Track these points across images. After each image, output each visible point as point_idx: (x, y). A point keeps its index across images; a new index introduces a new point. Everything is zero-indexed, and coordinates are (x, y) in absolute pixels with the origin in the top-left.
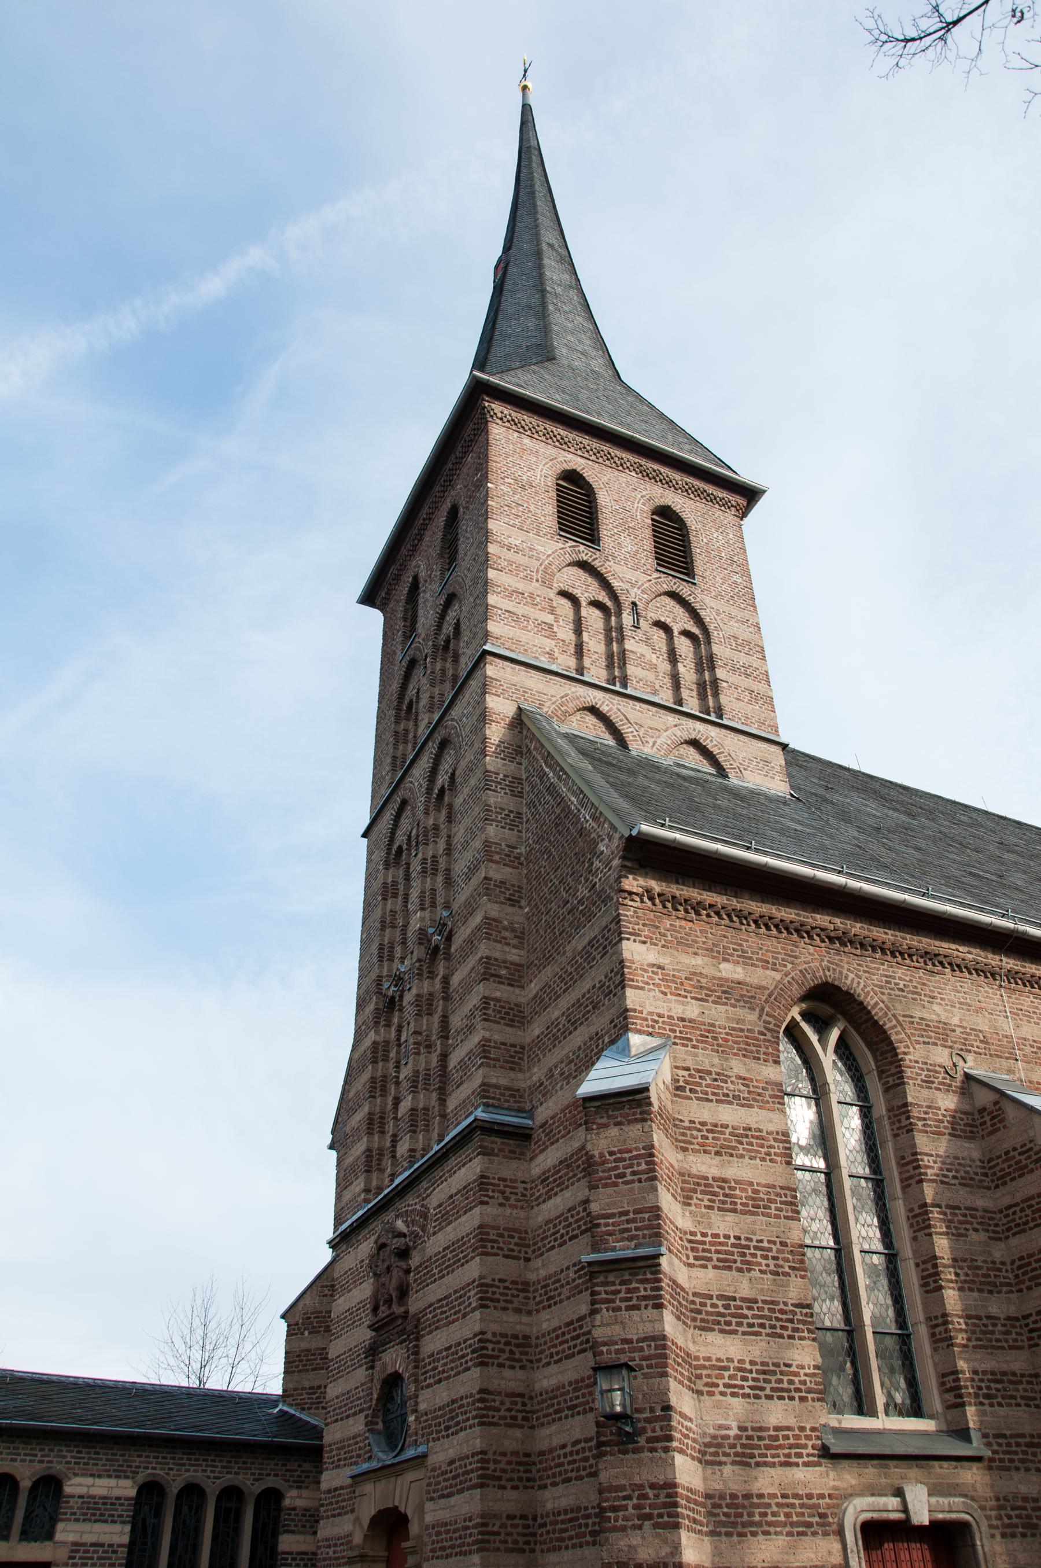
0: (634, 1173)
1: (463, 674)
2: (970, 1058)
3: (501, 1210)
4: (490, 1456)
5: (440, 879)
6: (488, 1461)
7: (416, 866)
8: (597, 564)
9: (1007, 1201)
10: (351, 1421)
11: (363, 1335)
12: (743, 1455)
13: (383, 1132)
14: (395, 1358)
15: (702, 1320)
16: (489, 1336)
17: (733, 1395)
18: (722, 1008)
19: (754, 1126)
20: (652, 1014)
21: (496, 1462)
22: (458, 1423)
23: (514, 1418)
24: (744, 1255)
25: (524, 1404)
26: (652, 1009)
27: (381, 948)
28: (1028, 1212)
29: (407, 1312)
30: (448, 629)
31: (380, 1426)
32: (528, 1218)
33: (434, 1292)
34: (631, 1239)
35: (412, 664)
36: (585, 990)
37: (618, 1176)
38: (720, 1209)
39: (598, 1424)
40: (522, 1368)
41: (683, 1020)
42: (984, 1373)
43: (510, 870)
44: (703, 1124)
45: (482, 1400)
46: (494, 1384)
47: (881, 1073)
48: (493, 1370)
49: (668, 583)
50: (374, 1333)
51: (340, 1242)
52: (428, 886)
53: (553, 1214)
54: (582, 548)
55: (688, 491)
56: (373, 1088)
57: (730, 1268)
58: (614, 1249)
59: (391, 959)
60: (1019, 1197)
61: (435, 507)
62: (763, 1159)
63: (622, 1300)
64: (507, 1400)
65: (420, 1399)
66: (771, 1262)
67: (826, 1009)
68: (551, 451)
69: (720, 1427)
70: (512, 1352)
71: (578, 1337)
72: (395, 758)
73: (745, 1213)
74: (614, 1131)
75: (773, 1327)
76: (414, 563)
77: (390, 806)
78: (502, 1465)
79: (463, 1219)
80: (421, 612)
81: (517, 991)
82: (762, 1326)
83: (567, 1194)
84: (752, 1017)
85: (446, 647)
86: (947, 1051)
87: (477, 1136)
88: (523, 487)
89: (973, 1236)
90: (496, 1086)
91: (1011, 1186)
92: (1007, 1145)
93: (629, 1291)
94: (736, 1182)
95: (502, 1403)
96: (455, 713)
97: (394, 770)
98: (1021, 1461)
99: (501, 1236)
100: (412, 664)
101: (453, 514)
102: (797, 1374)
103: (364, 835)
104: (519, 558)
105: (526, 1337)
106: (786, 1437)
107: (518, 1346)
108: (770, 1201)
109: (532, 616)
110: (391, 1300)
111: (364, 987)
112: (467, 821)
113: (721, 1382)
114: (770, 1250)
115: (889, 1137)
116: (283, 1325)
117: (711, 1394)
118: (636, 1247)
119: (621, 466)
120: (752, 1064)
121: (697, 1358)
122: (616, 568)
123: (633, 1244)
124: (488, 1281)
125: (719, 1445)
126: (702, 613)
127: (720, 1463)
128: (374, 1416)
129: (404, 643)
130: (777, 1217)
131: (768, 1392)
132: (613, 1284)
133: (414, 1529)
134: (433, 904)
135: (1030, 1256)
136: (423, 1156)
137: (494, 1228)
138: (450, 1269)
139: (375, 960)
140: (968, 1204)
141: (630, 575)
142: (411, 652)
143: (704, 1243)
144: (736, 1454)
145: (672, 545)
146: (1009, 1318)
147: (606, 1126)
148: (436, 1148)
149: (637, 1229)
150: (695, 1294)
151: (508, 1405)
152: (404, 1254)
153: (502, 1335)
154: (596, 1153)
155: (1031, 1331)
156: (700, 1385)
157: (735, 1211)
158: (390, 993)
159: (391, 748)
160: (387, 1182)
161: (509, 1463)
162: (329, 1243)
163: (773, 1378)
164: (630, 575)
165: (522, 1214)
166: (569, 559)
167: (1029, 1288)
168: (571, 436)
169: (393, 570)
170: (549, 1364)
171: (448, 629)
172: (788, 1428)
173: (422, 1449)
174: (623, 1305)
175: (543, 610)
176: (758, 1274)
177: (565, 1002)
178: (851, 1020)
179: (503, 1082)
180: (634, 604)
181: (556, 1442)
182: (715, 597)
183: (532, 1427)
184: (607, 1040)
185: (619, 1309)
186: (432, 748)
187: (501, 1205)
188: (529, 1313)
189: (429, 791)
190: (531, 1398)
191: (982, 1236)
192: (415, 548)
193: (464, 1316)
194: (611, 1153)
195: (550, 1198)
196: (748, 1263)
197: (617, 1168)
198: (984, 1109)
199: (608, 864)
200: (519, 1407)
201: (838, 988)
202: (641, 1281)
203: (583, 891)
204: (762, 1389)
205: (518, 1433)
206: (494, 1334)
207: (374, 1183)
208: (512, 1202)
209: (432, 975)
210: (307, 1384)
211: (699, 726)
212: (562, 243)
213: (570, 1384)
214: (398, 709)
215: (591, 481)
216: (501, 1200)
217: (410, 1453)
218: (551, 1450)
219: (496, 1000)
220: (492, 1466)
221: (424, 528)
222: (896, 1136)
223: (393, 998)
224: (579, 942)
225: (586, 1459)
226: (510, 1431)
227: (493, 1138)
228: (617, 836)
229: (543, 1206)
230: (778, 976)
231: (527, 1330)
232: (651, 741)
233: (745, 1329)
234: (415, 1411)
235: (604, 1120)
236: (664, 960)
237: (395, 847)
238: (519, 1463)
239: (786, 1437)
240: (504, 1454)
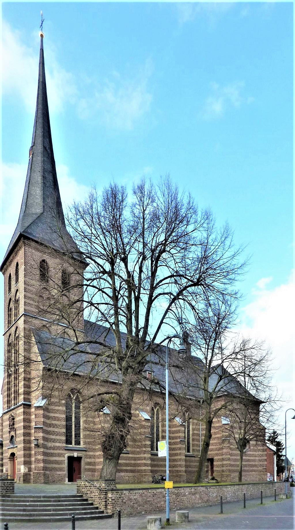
14: (13, 433)
133: (16, 455)
212: (32, 188)
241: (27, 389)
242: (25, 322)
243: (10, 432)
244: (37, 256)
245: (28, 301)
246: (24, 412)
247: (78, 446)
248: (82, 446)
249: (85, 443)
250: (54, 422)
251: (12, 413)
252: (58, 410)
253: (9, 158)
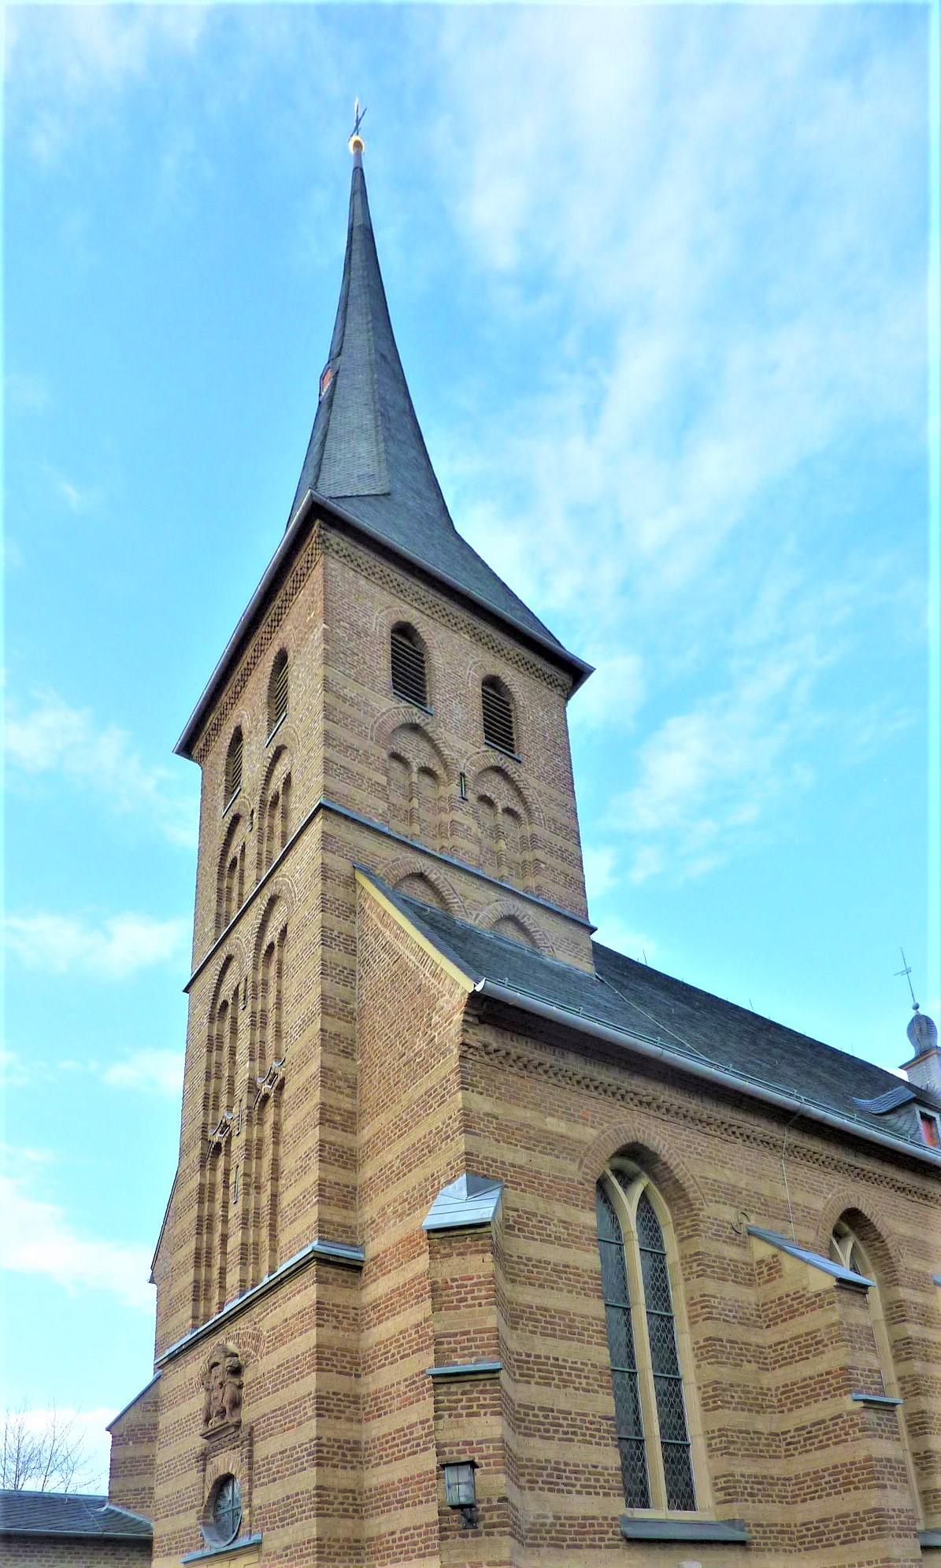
0: (473, 1298)
1: (294, 828)
2: (753, 1217)
3: (334, 1332)
4: (325, 1542)
5: (270, 1031)
6: (323, 1546)
7: (244, 1019)
8: (429, 729)
9: (777, 1338)
10: (182, 1516)
11: (196, 1442)
12: (557, 1539)
13: (209, 1266)
14: (227, 1461)
15: (526, 1428)
16: (324, 1441)
17: (550, 1490)
18: (547, 1158)
19: (572, 1264)
20: (486, 1158)
21: (330, 1547)
22: (293, 1516)
23: (346, 1510)
24: (561, 1374)
25: (355, 1499)
26: (487, 1154)
27: (206, 1097)
28: (796, 1348)
30: (277, 784)
31: (211, 1520)
32: (358, 1340)
33: (267, 1404)
34: (472, 1355)
35: (236, 819)
36: (421, 1136)
37: (461, 1301)
38: (542, 1334)
39: (440, 1513)
40: (353, 1468)
41: (514, 1166)
42: (750, 1476)
43: (343, 1023)
44: (529, 1259)
45: (318, 1496)
46: (329, 1482)
47: (677, 1225)
48: (328, 1470)
49: (495, 758)
51: (168, 1362)
52: (258, 1038)
53: (384, 1337)
54: (415, 710)
55: (518, 663)
56: (199, 1226)
57: (549, 1385)
58: (455, 1364)
59: (216, 1108)
60: (787, 1336)
61: (260, 651)
62: (578, 1293)
63: (463, 1408)
64: (340, 1496)
65: (254, 1495)
66: (584, 1381)
67: (631, 1166)
68: (385, 597)
69: (539, 1516)
70: (344, 1455)
71: (408, 1441)
72: (218, 915)
73: (562, 1338)
74: (456, 1260)
75: (584, 1435)
76: (235, 713)
77: (213, 961)
78: (336, 1549)
79: (298, 1339)
80: (245, 766)
81: (350, 1136)
82: (574, 1433)
83: (399, 1318)
84: (573, 1167)
85: (274, 803)
86: (734, 1210)
87: (313, 1268)
88: (358, 634)
89: (747, 1366)
90: (331, 1223)
91: (782, 1326)
92: (781, 1292)
93: (470, 1400)
94: (556, 1311)
95: (336, 1498)
96: (285, 868)
97: (218, 927)
98: (773, 1544)
99: (335, 1355)
100: (236, 819)
101: (282, 659)
102: (602, 1474)
104: (353, 711)
105: (356, 1442)
106: (592, 1525)
107: (350, 1450)
108: (584, 1329)
109: (367, 775)
110: (224, 1411)
111: (187, 1135)
112: (301, 975)
113: (540, 1480)
114: (582, 1370)
115: (681, 1281)
116: (109, 1437)
117: (532, 1489)
118: (477, 1362)
119: (455, 627)
120: (573, 1210)
121: (521, 1459)
122: (446, 735)
123: (473, 1359)
124: (324, 1394)
125: (539, 1531)
126: (525, 792)
127: (538, 1546)
128: (205, 1511)
129: (226, 798)
130: (589, 1343)
131: (578, 1488)
132: (456, 1393)
134: (263, 1056)
135: (793, 1384)
136: (253, 1286)
137: (328, 1347)
138: (285, 1384)
139: (200, 1108)
140: (745, 1340)
141: (460, 745)
142: (235, 808)
143: (528, 1362)
144: (552, 1538)
145: (498, 721)
146: (771, 1434)
147: (449, 1255)
148: (266, 1280)
149: (477, 1347)
150: (520, 1405)
151: (341, 1500)
152: (237, 1371)
153: (335, 1440)
154: (439, 1280)
155: (789, 1444)
156: (523, 1481)
157: (554, 1336)
158: (216, 1139)
159: (214, 904)
160: (214, 1309)
161: (342, 1547)
163: (583, 1477)
164: (460, 745)
165: (353, 1336)
166: (401, 720)
167: (791, 1410)
168: (408, 585)
170: (378, 1464)
171: (277, 784)
172: (594, 1518)
173: (256, 1538)
174: (464, 1412)
175: (376, 769)
176: (572, 1391)
177: (400, 1146)
178: (654, 1177)
179: (337, 1219)
180: (462, 775)
181: (384, 1529)
182: (538, 778)
183: (362, 1518)
184: (443, 1180)
185: (461, 1416)
186: (261, 903)
187: (335, 1327)
188: (359, 1421)
189: (258, 946)
190: (360, 1493)
191: (754, 1366)
192: (237, 695)
193: (300, 1424)
194: (454, 1280)
195: (381, 1322)
196: (564, 1381)
197: (459, 1293)
198: (762, 1261)
199: (448, 1019)
200: (350, 1501)
201: (646, 1149)
202: (482, 1392)
203: (420, 1044)
204: (574, 1486)
205: (349, 1523)
206: (329, 1440)
207: (202, 1310)
208: (345, 1325)
209: (261, 1122)
210: (132, 1487)
211: (518, 904)
213: (400, 1481)
214: (221, 866)
215: (425, 637)
216: (335, 1323)
217: (243, 1541)
218: (379, 1537)
219: (330, 1143)
220: (327, 1550)
221: (248, 673)
222: (687, 1280)
223: (218, 1144)
224: (416, 1091)
225: (415, 1544)
226: (343, 1521)
227: (328, 1269)
228: (459, 992)
229: (373, 1330)
230: (594, 1132)
231: (356, 1436)
232: (475, 913)
233: (561, 1435)
235: (448, 1250)
236: (495, 1111)
237: (220, 1002)
238: (350, 1548)
239: (592, 1525)
240: (338, 1540)
241: (337, 1174)
242: (327, 841)
243: (204, 1457)
244: (380, 605)
245: (342, 760)
246: (320, 1307)
247: (640, 1513)
248: (708, 1506)
249: (728, 1490)
250: (544, 1346)
251: (228, 1340)
252: (561, 1270)
253: (65, 852)
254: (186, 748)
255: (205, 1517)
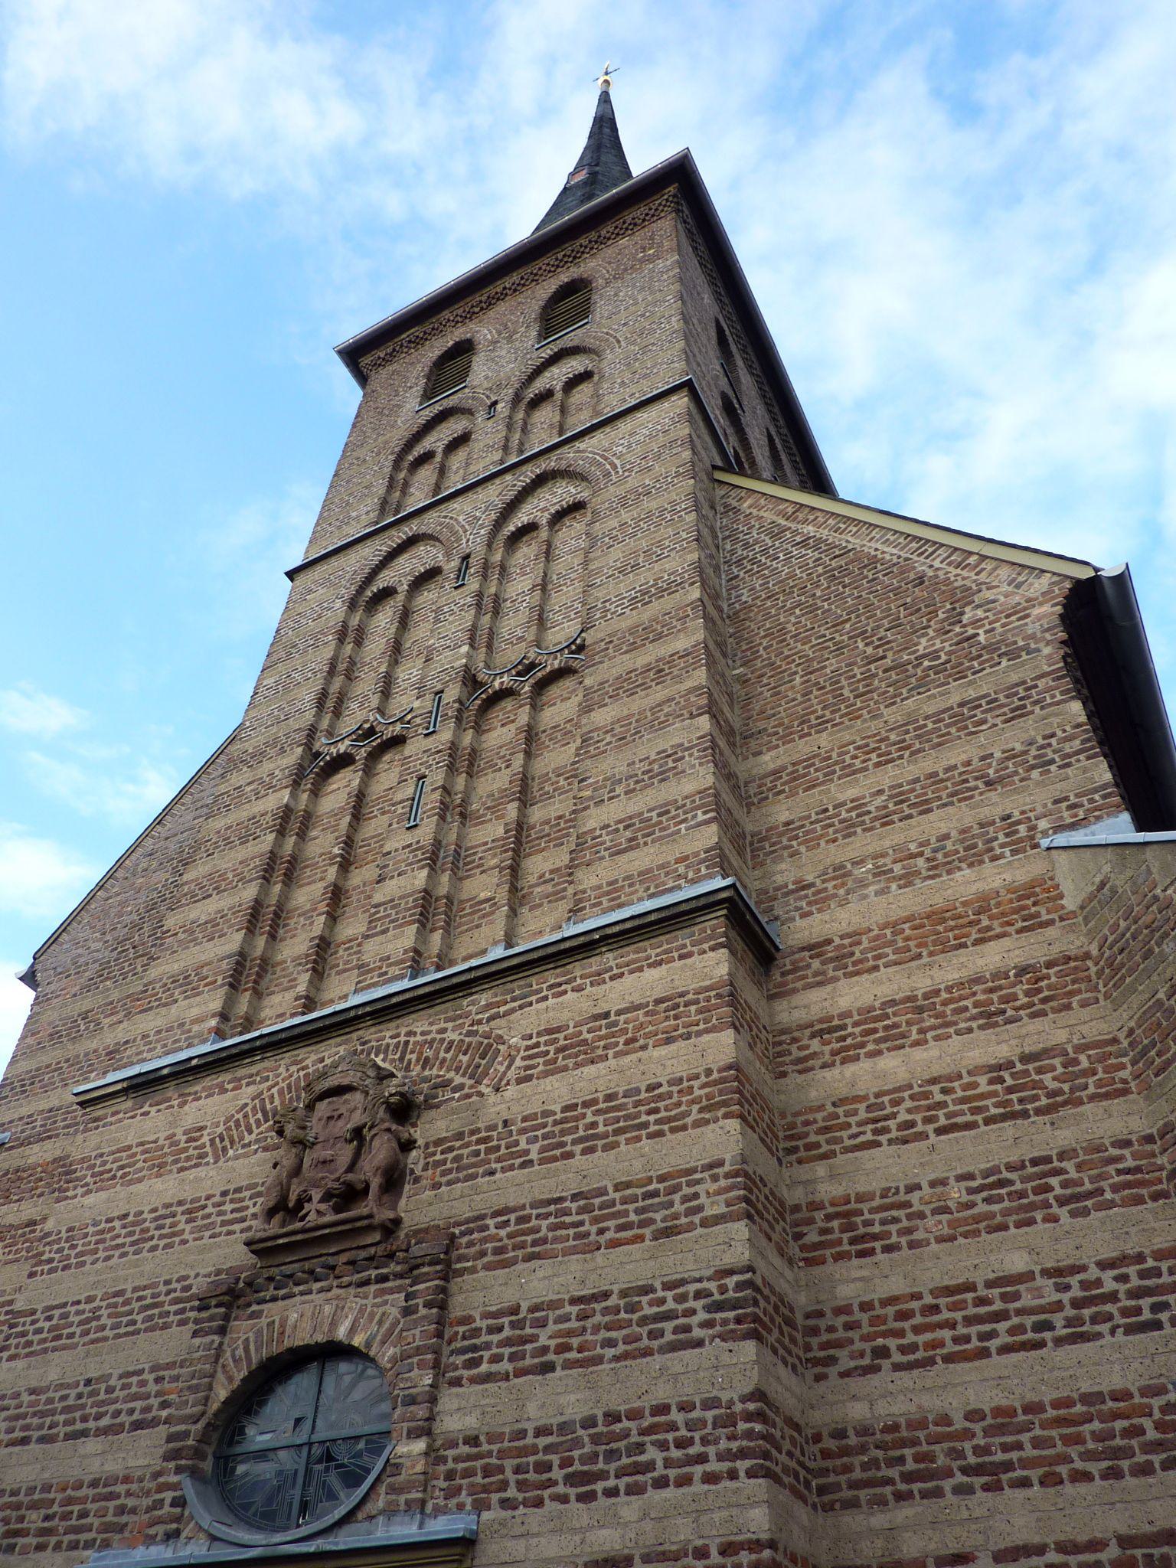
29: (397, 1222)
31: (207, 1465)
50: (253, 1259)
77: (393, 532)
103: (291, 575)
136: (439, 968)
152: (404, 1110)
162: (1122, 581)
169: (416, 331)
186: (530, 472)
229: (820, 1074)
234: (425, 1430)
254: (358, 356)
255: (198, 1454)
